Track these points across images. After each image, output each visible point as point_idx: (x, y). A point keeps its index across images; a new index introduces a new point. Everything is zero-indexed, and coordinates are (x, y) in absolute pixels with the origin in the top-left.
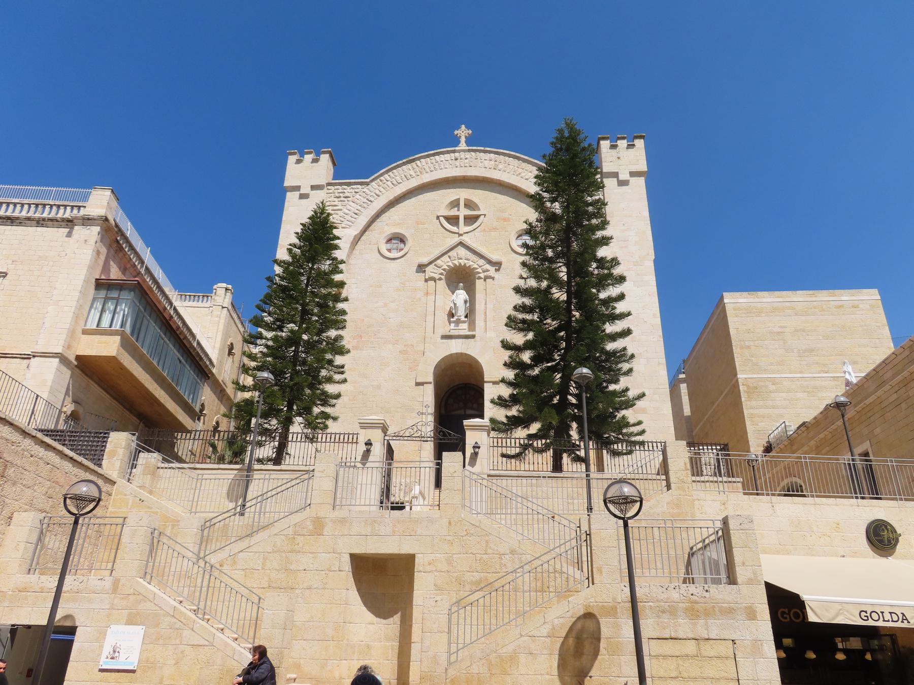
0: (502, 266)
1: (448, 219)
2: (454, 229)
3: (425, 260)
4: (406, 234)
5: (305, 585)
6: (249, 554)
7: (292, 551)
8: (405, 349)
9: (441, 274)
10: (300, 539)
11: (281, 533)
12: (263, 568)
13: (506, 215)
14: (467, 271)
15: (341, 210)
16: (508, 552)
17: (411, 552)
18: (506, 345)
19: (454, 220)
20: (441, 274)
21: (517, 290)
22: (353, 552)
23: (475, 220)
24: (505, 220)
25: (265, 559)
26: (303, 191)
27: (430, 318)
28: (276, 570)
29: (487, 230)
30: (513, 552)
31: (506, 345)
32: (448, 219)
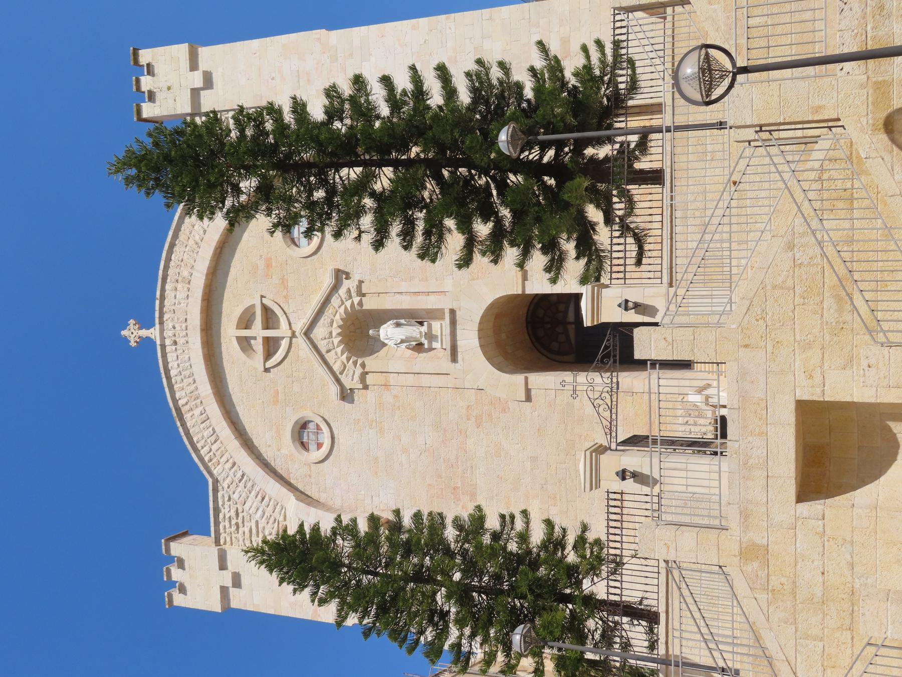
0: (341, 268)
1: (268, 355)
2: (284, 344)
3: (334, 390)
4: (294, 418)
5: (847, 572)
6: (799, 660)
7: (794, 593)
8: (474, 419)
9: (355, 363)
10: (774, 582)
11: (765, 612)
12: (821, 640)
13: (261, 264)
14: (349, 323)
15: (257, 522)
16: (790, 254)
17: (792, 406)
18: (465, 261)
19: (271, 346)
20: (355, 363)
21: (378, 245)
22: (793, 498)
23: (269, 313)
24: (268, 266)
25: (806, 636)
26: (228, 583)
27: (426, 381)
28: (823, 620)
29: (285, 293)
30: (791, 247)
31: (465, 261)
32: (268, 355)
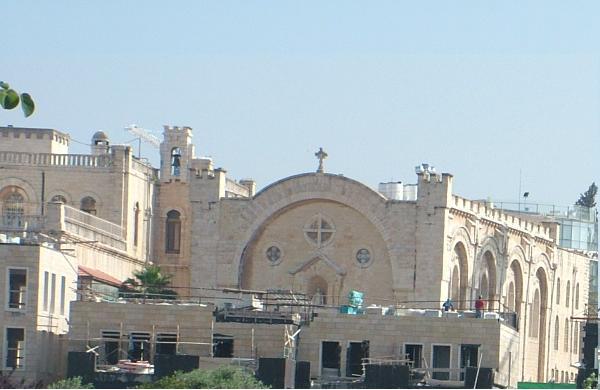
13: (350, 234)
